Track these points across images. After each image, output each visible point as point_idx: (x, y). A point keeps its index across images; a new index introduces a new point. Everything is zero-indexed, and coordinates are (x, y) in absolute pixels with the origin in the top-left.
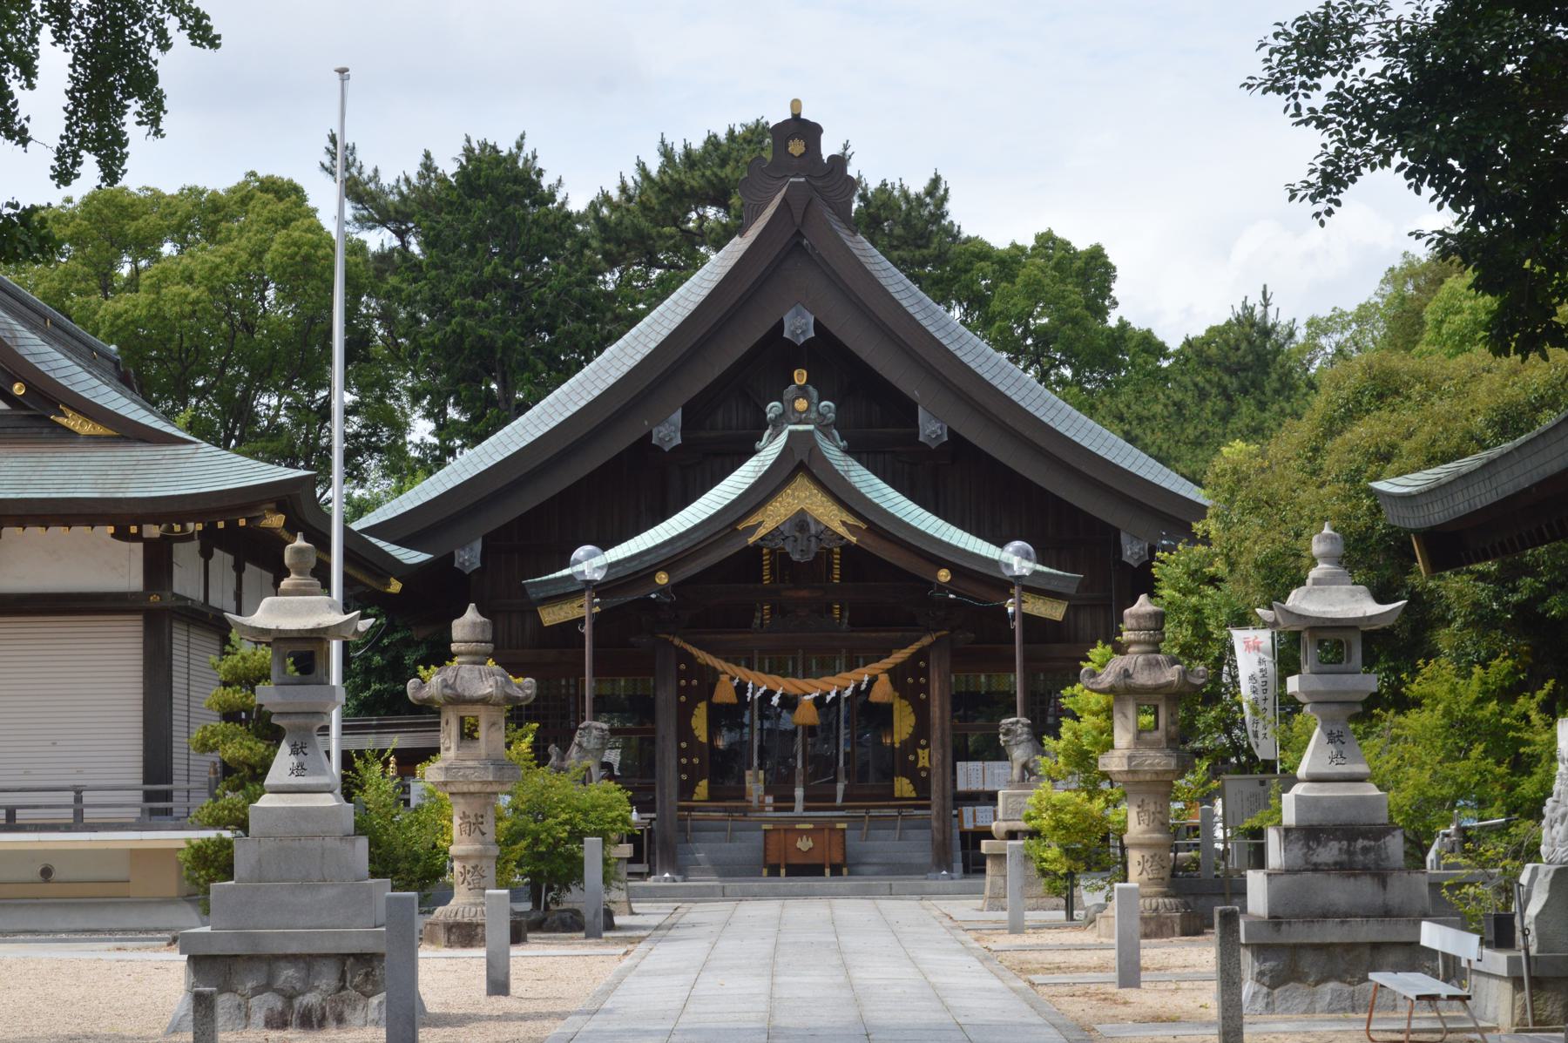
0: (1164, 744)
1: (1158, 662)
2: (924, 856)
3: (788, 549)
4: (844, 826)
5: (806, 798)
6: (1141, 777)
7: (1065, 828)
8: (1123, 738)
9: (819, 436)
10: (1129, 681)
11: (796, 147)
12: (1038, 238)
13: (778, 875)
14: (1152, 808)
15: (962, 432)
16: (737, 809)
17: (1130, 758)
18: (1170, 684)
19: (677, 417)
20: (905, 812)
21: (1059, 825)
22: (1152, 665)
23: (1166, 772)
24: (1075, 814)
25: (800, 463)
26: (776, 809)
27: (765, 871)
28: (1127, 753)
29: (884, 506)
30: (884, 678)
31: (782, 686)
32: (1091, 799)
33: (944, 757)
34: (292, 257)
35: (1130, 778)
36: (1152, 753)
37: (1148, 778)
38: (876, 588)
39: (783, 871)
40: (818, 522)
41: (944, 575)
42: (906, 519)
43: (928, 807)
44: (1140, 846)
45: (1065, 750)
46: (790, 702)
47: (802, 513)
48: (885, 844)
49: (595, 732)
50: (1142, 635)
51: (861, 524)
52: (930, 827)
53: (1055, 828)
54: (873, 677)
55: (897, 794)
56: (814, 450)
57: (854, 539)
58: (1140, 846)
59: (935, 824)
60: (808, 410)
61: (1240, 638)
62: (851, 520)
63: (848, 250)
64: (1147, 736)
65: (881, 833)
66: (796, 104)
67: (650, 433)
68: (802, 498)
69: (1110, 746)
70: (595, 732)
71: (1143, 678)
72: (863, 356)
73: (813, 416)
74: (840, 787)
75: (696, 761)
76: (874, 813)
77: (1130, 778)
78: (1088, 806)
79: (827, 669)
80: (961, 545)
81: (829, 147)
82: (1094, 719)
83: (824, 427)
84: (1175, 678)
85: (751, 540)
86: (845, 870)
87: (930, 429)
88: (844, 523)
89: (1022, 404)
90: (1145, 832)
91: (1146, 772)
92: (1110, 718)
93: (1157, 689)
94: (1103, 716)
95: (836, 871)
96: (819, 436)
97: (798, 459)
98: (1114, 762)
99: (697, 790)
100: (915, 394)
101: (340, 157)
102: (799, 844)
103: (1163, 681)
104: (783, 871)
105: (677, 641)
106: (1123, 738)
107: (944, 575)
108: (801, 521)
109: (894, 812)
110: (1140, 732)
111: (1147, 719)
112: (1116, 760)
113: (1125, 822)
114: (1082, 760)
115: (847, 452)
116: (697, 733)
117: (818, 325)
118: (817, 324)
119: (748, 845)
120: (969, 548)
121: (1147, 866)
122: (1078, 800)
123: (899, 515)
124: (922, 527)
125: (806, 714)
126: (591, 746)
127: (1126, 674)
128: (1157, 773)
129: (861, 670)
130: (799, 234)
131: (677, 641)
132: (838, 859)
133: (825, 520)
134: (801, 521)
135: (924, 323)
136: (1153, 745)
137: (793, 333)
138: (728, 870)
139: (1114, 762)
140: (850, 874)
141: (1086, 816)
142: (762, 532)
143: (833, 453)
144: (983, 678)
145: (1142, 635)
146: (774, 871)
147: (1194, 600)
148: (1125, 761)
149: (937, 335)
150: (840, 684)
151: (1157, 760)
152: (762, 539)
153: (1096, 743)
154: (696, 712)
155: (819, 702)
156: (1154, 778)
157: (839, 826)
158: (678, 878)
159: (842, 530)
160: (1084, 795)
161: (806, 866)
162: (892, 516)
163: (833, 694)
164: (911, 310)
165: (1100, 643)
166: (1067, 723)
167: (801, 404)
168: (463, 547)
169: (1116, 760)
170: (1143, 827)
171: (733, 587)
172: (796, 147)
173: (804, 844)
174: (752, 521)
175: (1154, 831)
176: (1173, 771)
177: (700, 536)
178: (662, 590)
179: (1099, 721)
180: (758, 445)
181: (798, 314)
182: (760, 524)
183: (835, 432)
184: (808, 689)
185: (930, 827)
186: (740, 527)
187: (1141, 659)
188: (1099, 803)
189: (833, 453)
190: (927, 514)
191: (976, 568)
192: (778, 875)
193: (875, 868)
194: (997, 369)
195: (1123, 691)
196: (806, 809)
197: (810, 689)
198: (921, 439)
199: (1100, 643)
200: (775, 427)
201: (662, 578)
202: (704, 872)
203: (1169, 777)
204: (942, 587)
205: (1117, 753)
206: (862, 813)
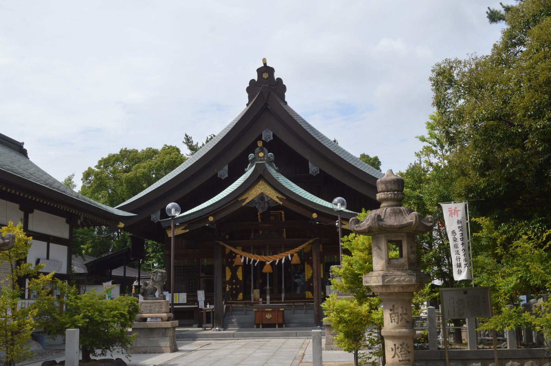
0: (407, 267)
1: (400, 211)
2: (312, 320)
3: (257, 207)
4: (283, 309)
5: (271, 299)
6: (392, 290)
7: (346, 322)
8: (378, 264)
9: (267, 165)
10: (381, 223)
11: (265, 76)
12: (361, 155)
13: (259, 327)
14: (400, 311)
15: (324, 170)
16: (249, 303)
17: (384, 277)
18: (410, 224)
19: (226, 168)
20: (307, 304)
21: (341, 321)
22: (397, 213)
23: (409, 286)
24: (351, 314)
25: (260, 176)
26: (263, 303)
27: (255, 326)
28: (382, 273)
29: (292, 190)
30: (295, 255)
31: (259, 259)
32: (361, 304)
33: (318, 283)
34: (171, 161)
35: (384, 290)
36: (399, 273)
37: (396, 290)
38: (295, 223)
39: (261, 326)
40: (268, 197)
41: (315, 215)
42: (300, 195)
43: (313, 302)
44: (393, 337)
45: (344, 273)
46: (262, 264)
47: (262, 193)
48: (300, 315)
49: (159, 274)
50: (389, 195)
51: (284, 197)
52: (313, 309)
53: (339, 322)
54: (290, 256)
55: (307, 297)
56: (265, 170)
57: (281, 203)
58: (393, 337)
59: (315, 308)
60: (264, 157)
61: (446, 207)
62: (280, 196)
63: (283, 108)
64: (395, 262)
65: (299, 311)
66: (264, 60)
67: (217, 174)
68: (262, 188)
69: (371, 269)
70: (159, 274)
71: (391, 221)
72: (290, 145)
73: (266, 158)
74: (283, 295)
75: (238, 286)
76: (296, 304)
77: (384, 290)
78: (359, 308)
79: (275, 253)
80: (320, 204)
81: (276, 76)
82: (361, 254)
83: (270, 163)
84: (414, 220)
85: (244, 204)
86: (284, 326)
87: (313, 169)
88: (277, 197)
89: (345, 159)
90: (395, 328)
91: (395, 286)
92: (370, 253)
93: (400, 228)
94: (366, 252)
95: (280, 326)
96: (267, 165)
97: (259, 174)
98: (372, 280)
99: (239, 296)
100: (308, 157)
101: (188, 141)
102: (267, 316)
103: (405, 222)
104: (261, 326)
105: (221, 243)
106: (378, 264)
107: (315, 215)
108: (262, 197)
109: (303, 304)
110: (389, 262)
111: (394, 254)
112: (374, 278)
113: (382, 319)
114: (355, 281)
115: (277, 171)
116: (239, 277)
117: (274, 135)
118: (274, 135)
119: (250, 317)
120: (324, 205)
121: (398, 351)
122: (352, 305)
123: (297, 193)
124: (306, 197)
125: (267, 269)
126: (157, 280)
127: (379, 218)
128: (402, 287)
129: (287, 252)
130: (266, 104)
131: (221, 243)
132: (281, 321)
133: (270, 196)
134: (262, 197)
135: (310, 132)
136: (400, 268)
137: (265, 138)
138: (243, 326)
139: (372, 280)
140: (286, 327)
141: (358, 314)
142: (247, 201)
143: (273, 171)
144: (336, 257)
145: (389, 195)
146: (258, 326)
147: (417, 193)
148: (380, 279)
149: (314, 136)
150: (281, 257)
151: (402, 278)
152: (247, 203)
153: (362, 268)
154: (239, 270)
155: (272, 264)
156: (401, 290)
157: (281, 309)
158: (221, 329)
159: (277, 200)
160: (356, 301)
161: (271, 324)
162: (295, 193)
163: (277, 261)
164: (305, 128)
165: (363, 210)
166: (344, 258)
167: (261, 154)
168: (153, 213)
169: (374, 278)
170: (394, 324)
171: (240, 222)
172: (265, 76)
173: (268, 316)
174: (244, 197)
175: (402, 327)
176: (414, 285)
177: (224, 202)
178: (212, 223)
179: (364, 255)
180: (246, 170)
181: (267, 131)
182: (247, 198)
183: (274, 164)
184: (268, 259)
185: (313, 309)
186: (240, 199)
187: (389, 209)
188: (365, 308)
189: (273, 171)
190: (308, 193)
191: (325, 212)
192: (259, 327)
193: (295, 324)
194: (336, 148)
195: (376, 232)
196: (271, 303)
197: (269, 260)
198: (310, 173)
199: (363, 210)
200: (252, 163)
201: (211, 219)
202: (234, 327)
203: (411, 289)
204: (314, 220)
205: (374, 273)
206: (292, 304)
